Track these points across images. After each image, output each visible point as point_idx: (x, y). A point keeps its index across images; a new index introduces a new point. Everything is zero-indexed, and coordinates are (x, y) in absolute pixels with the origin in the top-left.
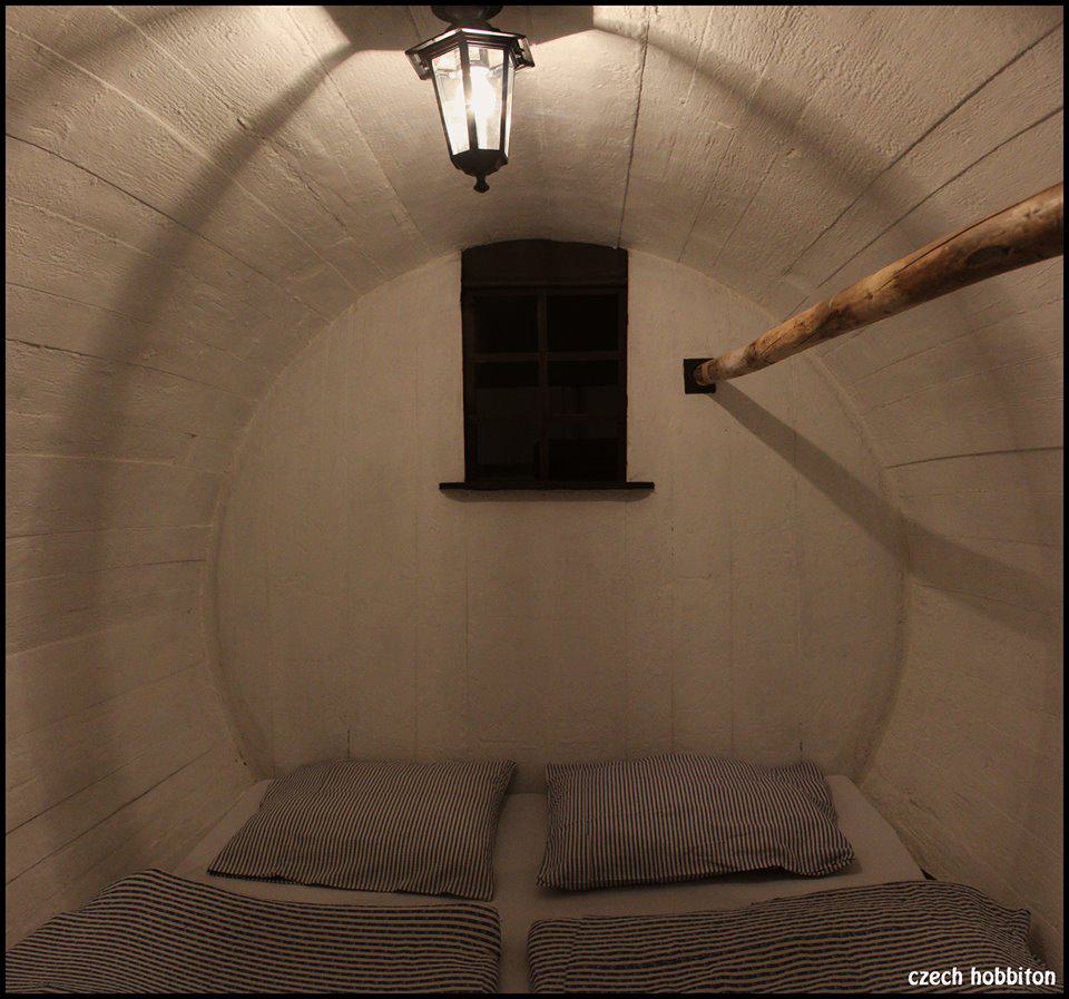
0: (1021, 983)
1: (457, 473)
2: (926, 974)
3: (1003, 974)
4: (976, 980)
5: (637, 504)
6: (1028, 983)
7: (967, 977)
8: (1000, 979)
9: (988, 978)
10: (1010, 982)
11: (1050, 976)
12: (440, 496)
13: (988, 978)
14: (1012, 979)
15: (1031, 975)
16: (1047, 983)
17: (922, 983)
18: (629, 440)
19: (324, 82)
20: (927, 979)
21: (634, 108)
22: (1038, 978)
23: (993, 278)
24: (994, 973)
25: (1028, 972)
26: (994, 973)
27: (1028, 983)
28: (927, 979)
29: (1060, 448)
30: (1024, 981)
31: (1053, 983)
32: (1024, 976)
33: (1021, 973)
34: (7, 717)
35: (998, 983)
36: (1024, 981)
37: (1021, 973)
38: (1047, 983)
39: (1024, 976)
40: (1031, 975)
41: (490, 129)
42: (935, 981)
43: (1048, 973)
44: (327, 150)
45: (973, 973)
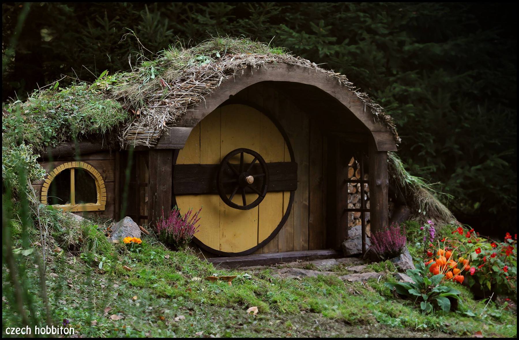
1: (181, 151)
2: (14, 329)
4: (37, 332)
7: (33, 330)
8: (49, 331)
9: (43, 331)
10: (47, 333)
11: (29, 330)
13: (43, 330)
14: (49, 332)
15: (63, 330)
17: (12, 333)
18: (182, 164)
19: (107, 131)
20: (14, 332)
22: (66, 331)
23: (277, 161)
26: (46, 329)
27: (62, 333)
28: (14, 332)
30: (60, 332)
32: (60, 330)
35: (53, 333)
36: (60, 332)
39: (60, 330)
45: (36, 329)
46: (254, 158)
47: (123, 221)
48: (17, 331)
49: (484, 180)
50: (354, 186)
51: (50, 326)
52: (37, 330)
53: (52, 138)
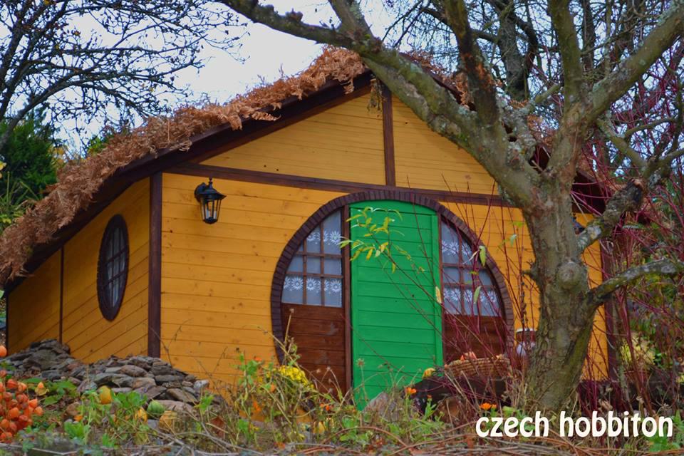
0: (626, 434)
2: (500, 421)
3: (602, 419)
6: (636, 434)
7: (554, 427)
8: (599, 428)
9: (583, 426)
11: (666, 424)
13: (583, 426)
16: (661, 434)
17: (494, 434)
21: (65, 281)
22: (649, 428)
24: (606, 420)
25: (636, 418)
26: (606, 420)
27: (636, 434)
29: (323, 302)
31: (546, 434)
32: (631, 423)
33: (626, 420)
37: (626, 420)
38: (661, 434)
39: (631, 423)
43: (662, 420)
44: (536, 94)
45: (563, 420)
46: (401, 182)
47: (313, 72)
48: (507, 428)
49: (553, 124)
50: (488, 129)
51: (602, 413)
52: (566, 423)
53: (642, 142)
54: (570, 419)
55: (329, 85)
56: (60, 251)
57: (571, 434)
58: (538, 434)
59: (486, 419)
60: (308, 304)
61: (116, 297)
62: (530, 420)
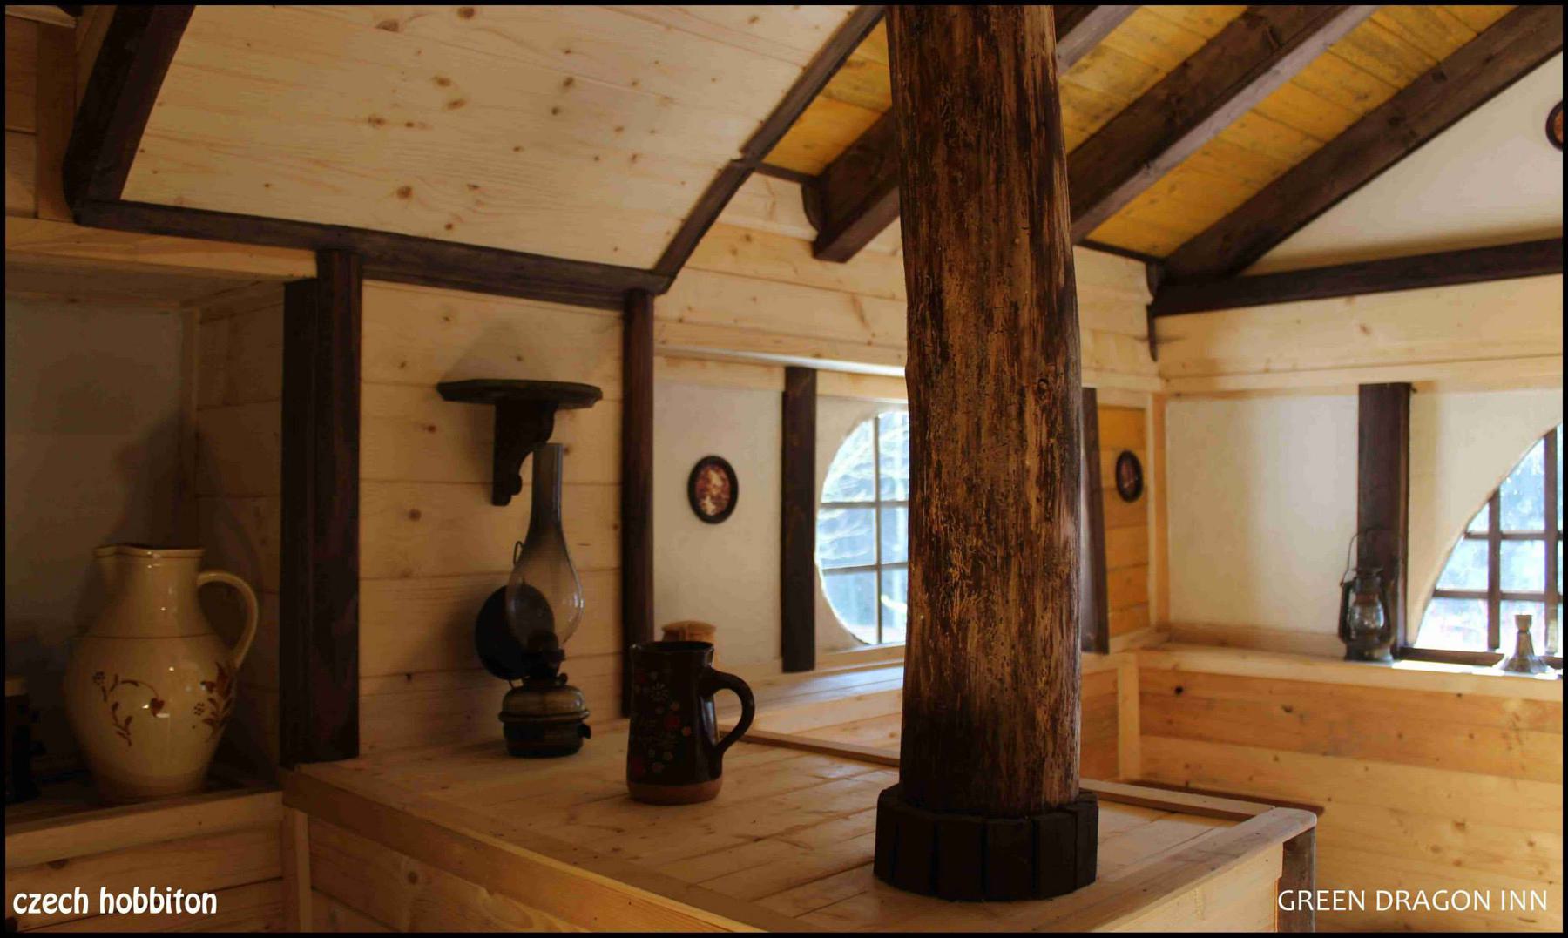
2: (37, 897)
3: (161, 897)
5: (803, 216)
6: (179, 910)
8: (157, 903)
11: (210, 901)
12: (438, 401)
13: (124, 903)
15: (183, 900)
17: (32, 910)
20: (39, 905)
22: (193, 903)
25: (179, 895)
27: (179, 910)
28: (39, 905)
31: (214, 910)
32: (173, 900)
34: (608, 931)
38: (169, 910)
39: (173, 900)
40: (183, 900)
41: (894, 531)
42: (50, 907)
43: (206, 896)
45: (103, 896)
48: (45, 904)
52: (107, 900)
54: (110, 896)
55: (221, 731)
56: (868, 426)
57: (111, 911)
58: (77, 911)
59: (24, 896)
60: (898, 756)
61: (1124, 471)
62: (69, 896)
